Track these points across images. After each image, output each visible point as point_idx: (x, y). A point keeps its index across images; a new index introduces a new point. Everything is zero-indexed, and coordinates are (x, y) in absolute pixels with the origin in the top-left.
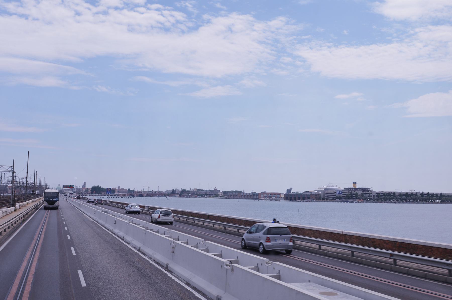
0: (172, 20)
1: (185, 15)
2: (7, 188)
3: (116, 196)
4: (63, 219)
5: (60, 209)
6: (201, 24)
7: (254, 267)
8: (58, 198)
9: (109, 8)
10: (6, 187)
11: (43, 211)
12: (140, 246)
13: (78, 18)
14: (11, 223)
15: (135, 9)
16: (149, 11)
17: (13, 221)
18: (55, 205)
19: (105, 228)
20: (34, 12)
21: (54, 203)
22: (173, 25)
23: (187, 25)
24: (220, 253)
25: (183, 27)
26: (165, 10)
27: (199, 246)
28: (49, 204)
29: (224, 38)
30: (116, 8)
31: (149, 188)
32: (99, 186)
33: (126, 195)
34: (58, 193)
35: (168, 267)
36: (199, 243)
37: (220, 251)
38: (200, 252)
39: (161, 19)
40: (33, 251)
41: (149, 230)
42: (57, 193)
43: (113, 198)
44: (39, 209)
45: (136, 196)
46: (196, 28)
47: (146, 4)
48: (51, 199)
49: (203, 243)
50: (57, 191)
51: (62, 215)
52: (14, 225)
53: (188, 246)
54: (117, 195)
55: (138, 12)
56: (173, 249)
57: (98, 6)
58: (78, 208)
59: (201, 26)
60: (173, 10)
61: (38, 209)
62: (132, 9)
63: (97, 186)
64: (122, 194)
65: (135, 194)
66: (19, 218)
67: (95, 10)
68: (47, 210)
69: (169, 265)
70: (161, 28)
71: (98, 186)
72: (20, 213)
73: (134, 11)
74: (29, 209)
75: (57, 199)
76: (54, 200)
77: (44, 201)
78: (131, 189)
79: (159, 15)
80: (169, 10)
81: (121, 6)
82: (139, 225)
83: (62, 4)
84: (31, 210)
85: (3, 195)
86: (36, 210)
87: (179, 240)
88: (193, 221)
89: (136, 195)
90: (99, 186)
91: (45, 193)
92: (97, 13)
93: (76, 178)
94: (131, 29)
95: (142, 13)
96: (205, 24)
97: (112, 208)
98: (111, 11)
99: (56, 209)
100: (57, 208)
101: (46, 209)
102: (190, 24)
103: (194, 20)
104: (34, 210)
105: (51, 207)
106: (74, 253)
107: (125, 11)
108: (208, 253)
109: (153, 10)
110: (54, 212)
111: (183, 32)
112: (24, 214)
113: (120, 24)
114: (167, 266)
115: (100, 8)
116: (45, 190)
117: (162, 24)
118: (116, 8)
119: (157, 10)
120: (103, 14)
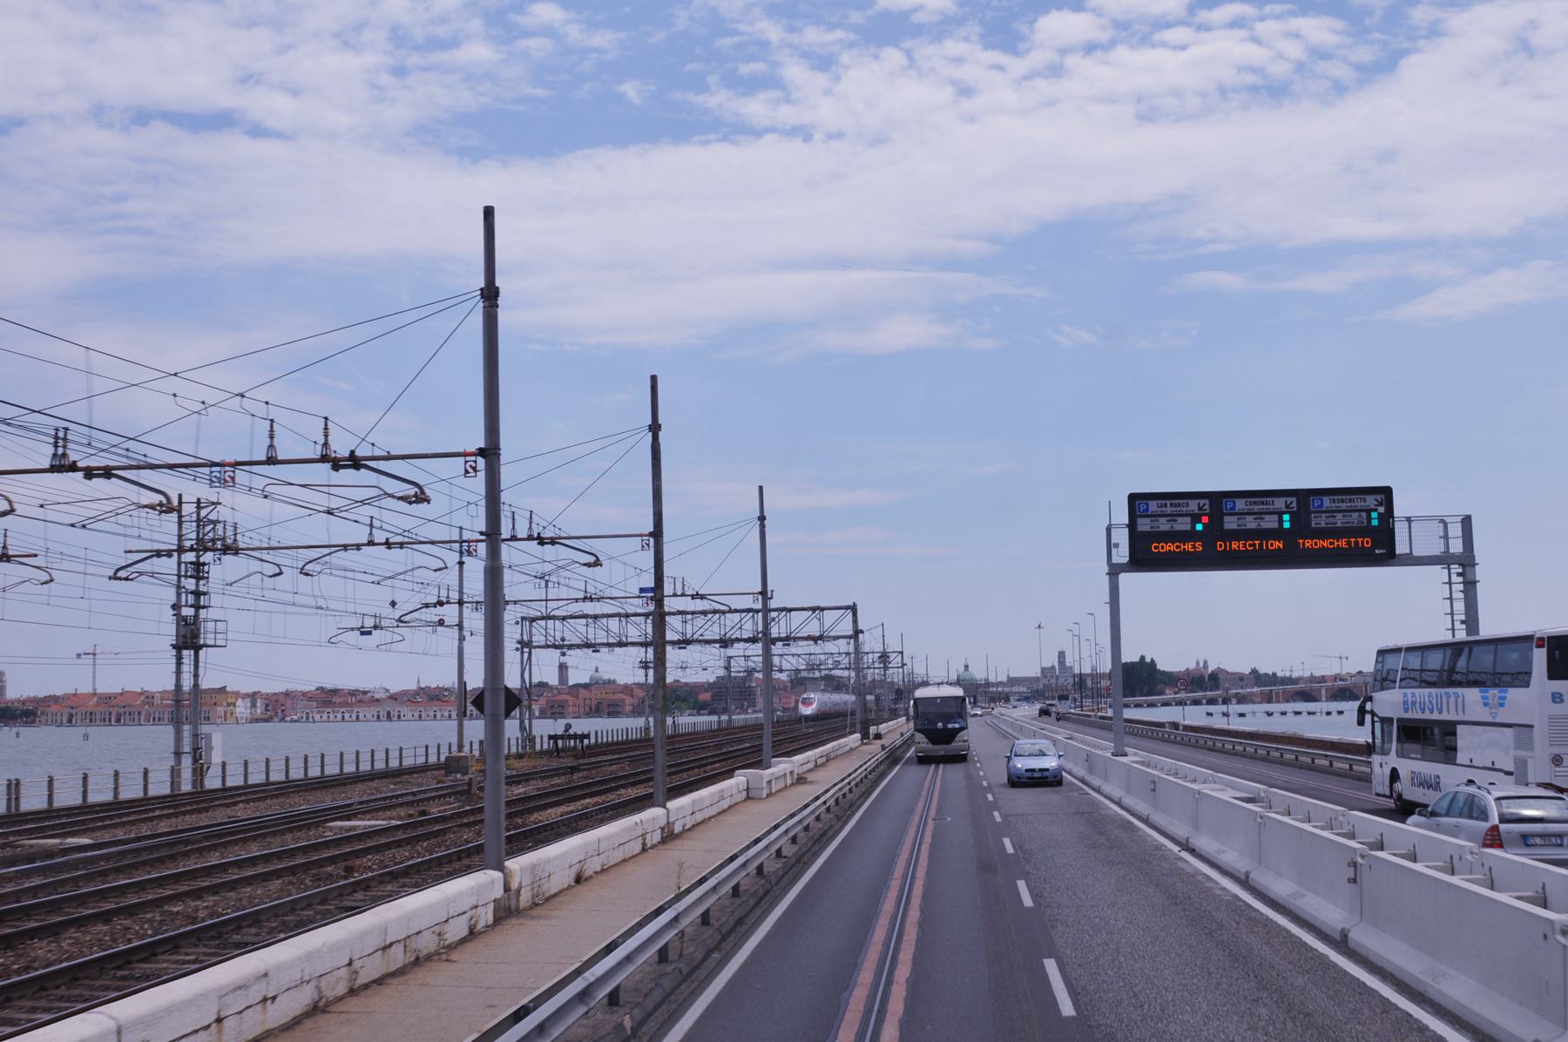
0: (1294, 50)
1: (1339, 25)
2: (749, 687)
3: (1234, 701)
4: (981, 773)
5: (976, 755)
6: (1406, 45)
7: (1322, 824)
8: (962, 717)
9: (1064, 51)
10: (747, 685)
11: (916, 771)
12: (1249, 869)
13: (967, 105)
14: (825, 803)
15: (1157, 37)
16: (1205, 36)
17: (845, 785)
18: (953, 744)
19: (1102, 794)
20: (826, 112)
21: (950, 736)
22: (1300, 67)
23: (1354, 58)
24: (1537, 892)
25: (1339, 71)
26: (1262, 19)
27: (1385, 844)
28: (934, 741)
29: (1505, 83)
30: (1090, 48)
31: (1344, 660)
32: (1148, 660)
33: (1277, 693)
34: (964, 699)
35: (1349, 941)
36: (1333, 820)
37: (1541, 885)
38: (1424, 875)
39: (1255, 54)
40: (910, 864)
41: (1275, 812)
42: (960, 701)
43: (1277, 716)
44: (904, 760)
45: (1324, 699)
46: (1386, 65)
47: (1191, 10)
48: (940, 724)
49: (1475, 858)
50: (959, 692)
51: (978, 765)
52: (849, 796)
53: (1418, 867)
54: (1236, 695)
55: (1164, 45)
56: (1353, 869)
57: (1028, 51)
58: (1146, 821)
59: (1405, 53)
60: (1294, 14)
61: (897, 764)
62: (1145, 41)
63: (1138, 660)
64: (1262, 693)
65: (1320, 690)
66: (849, 787)
67: (1017, 66)
68: (933, 767)
69: (1350, 935)
70: (1254, 90)
71: (1143, 658)
72: (839, 779)
73: (1154, 46)
74: (865, 763)
75: (961, 720)
76: (950, 726)
77: (916, 730)
78: (1262, 671)
79: (1242, 40)
80: (1277, 17)
81: (1102, 37)
82: (1194, 781)
83: (910, 67)
84: (874, 765)
85: (730, 721)
86: (890, 768)
87: (1384, 848)
88: (1327, 763)
89: (1323, 692)
90: (1148, 660)
91: (914, 703)
92: (1028, 77)
93: (1039, 626)
94: (1148, 111)
95: (1183, 48)
96: (1422, 43)
97: (1272, 774)
98: (1073, 61)
99: (960, 758)
100: (966, 755)
101: (924, 760)
102: (1364, 54)
103: (1376, 35)
104: (881, 767)
105: (942, 753)
106: (1028, 901)
107: (1123, 53)
108: (1544, 910)
109: (1219, 28)
110: (954, 772)
111: (1340, 89)
112: (863, 775)
113: (1110, 99)
114: (1345, 934)
115: (1037, 58)
116: (917, 691)
117: (1253, 70)
118: (1090, 48)
119: (1235, 24)
120: (1046, 77)
